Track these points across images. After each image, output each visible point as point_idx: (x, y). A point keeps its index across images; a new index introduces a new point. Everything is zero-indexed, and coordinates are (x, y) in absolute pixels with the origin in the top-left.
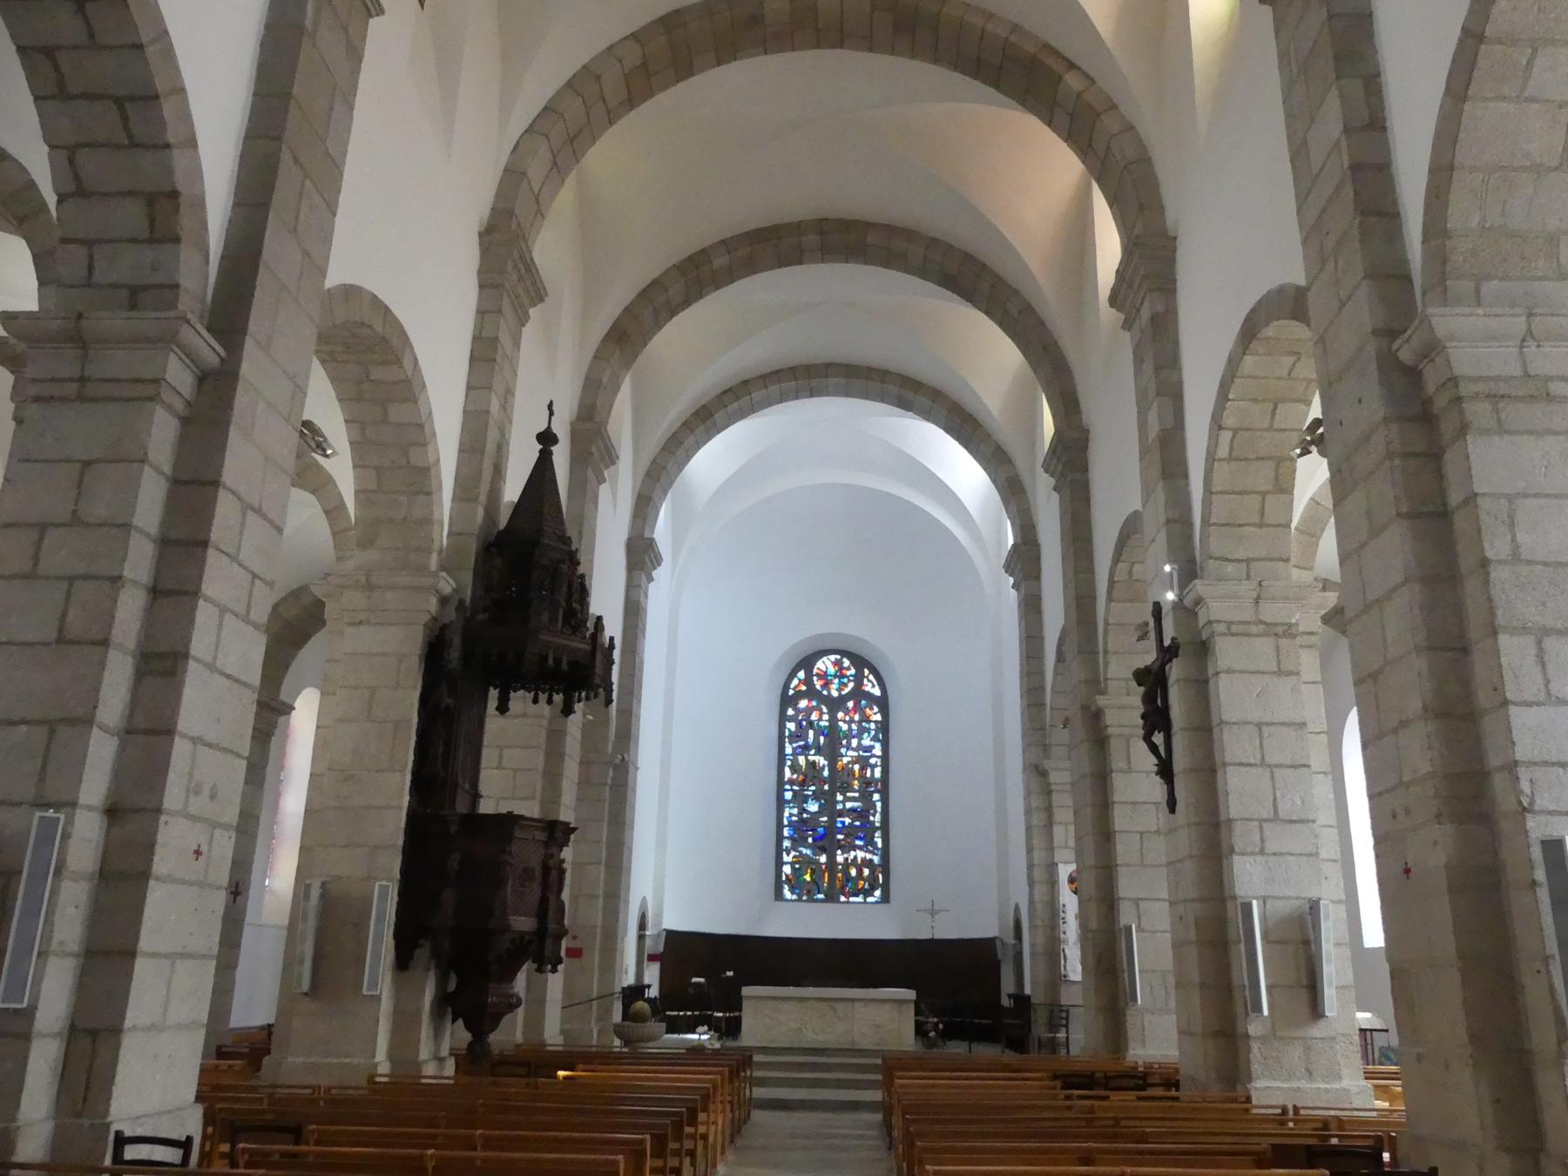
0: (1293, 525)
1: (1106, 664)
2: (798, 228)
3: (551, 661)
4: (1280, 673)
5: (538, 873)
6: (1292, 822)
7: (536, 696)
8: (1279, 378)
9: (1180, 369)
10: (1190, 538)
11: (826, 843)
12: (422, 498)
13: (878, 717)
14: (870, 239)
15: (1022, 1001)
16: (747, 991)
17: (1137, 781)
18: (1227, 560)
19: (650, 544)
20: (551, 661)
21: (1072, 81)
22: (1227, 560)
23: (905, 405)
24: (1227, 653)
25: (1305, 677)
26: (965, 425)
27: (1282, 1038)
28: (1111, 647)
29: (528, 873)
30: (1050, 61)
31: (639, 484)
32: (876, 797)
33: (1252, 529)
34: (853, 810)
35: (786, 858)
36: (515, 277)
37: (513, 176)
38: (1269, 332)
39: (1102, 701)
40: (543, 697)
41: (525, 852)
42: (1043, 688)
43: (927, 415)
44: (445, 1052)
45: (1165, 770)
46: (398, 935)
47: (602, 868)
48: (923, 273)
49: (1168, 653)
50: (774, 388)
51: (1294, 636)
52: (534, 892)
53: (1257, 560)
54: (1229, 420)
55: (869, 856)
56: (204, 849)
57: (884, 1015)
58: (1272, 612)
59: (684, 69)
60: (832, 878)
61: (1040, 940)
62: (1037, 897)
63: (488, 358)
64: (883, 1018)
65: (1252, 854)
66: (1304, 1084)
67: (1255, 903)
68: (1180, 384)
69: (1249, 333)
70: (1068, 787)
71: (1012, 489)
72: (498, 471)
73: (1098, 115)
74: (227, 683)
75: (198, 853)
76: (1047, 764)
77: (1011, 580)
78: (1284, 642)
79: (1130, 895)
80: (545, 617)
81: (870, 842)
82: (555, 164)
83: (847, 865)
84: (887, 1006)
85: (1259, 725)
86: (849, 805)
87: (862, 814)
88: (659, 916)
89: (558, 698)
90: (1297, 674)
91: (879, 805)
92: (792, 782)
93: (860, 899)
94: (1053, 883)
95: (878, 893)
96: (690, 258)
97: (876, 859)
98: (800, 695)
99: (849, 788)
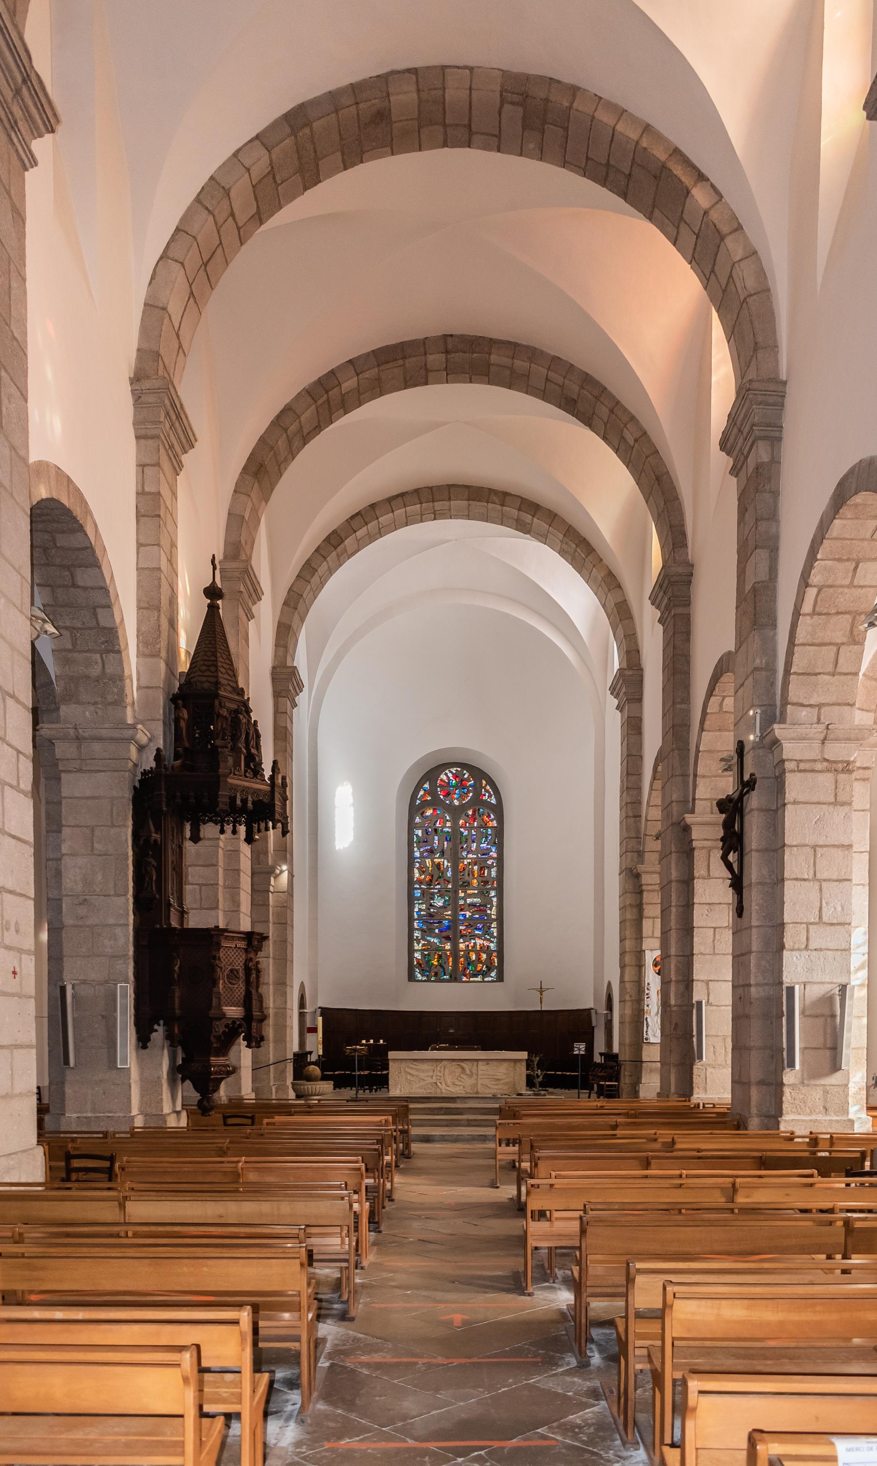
0: (861, 674)
1: (695, 786)
2: (422, 346)
3: (239, 802)
4: (836, 803)
5: (241, 974)
6: (832, 924)
7: (222, 827)
8: (863, 540)
9: (778, 522)
10: (773, 684)
11: (451, 934)
12: (111, 656)
13: (495, 824)
14: (494, 358)
15: (610, 1057)
16: (392, 1055)
17: (712, 891)
18: (802, 705)
19: (294, 671)
20: (239, 802)
21: (700, 196)
22: (802, 705)
23: (523, 528)
24: (795, 786)
25: (856, 805)
26: (579, 547)
27: (808, 1086)
28: (700, 771)
29: (233, 973)
30: (678, 170)
31: (278, 613)
32: (493, 893)
33: (827, 678)
34: (473, 905)
35: (416, 947)
36: (167, 425)
37: (153, 309)
38: (858, 499)
39: (689, 818)
40: (229, 828)
41: (231, 956)
42: (640, 803)
43: (543, 538)
44: (179, 1108)
45: (737, 884)
46: (138, 1023)
47: (271, 960)
48: (544, 395)
49: (747, 785)
50: (400, 512)
51: (850, 772)
52: (240, 988)
53: (828, 705)
54: (815, 578)
55: (486, 943)
56: (18, 970)
57: (502, 1071)
58: (834, 751)
59: (310, 176)
60: (456, 962)
61: (628, 1012)
62: (627, 978)
63: (152, 510)
64: (498, 1073)
65: (799, 950)
66: (820, 1117)
67: (797, 987)
68: (777, 537)
69: (840, 499)
70: (657, 887)
71: (621, 615)
72: (173, 624)
73: (722, 238)
74: (13, 841)
75: (14, 973)
76: (641, 868)
77: (616, 702)
78: (842, 777)
79: (702, 978)
80: (230, 760)
81: (487, 931)
82: (192, 293)
83: (467, 951)
84: (505, 1064)
85: (814, 848)
86: (469, 901)
87: (481, 909)
88: (315, 998)
89: (242, 829)
90: (850, 804)
91: (495, 899)
92: (420, 882)
93: (479, 979)
94: (640, 966)
95: (493, 974)
96: (319, 382)
97: (493, 946)
98: (425, 804)
99: (466, 885)
